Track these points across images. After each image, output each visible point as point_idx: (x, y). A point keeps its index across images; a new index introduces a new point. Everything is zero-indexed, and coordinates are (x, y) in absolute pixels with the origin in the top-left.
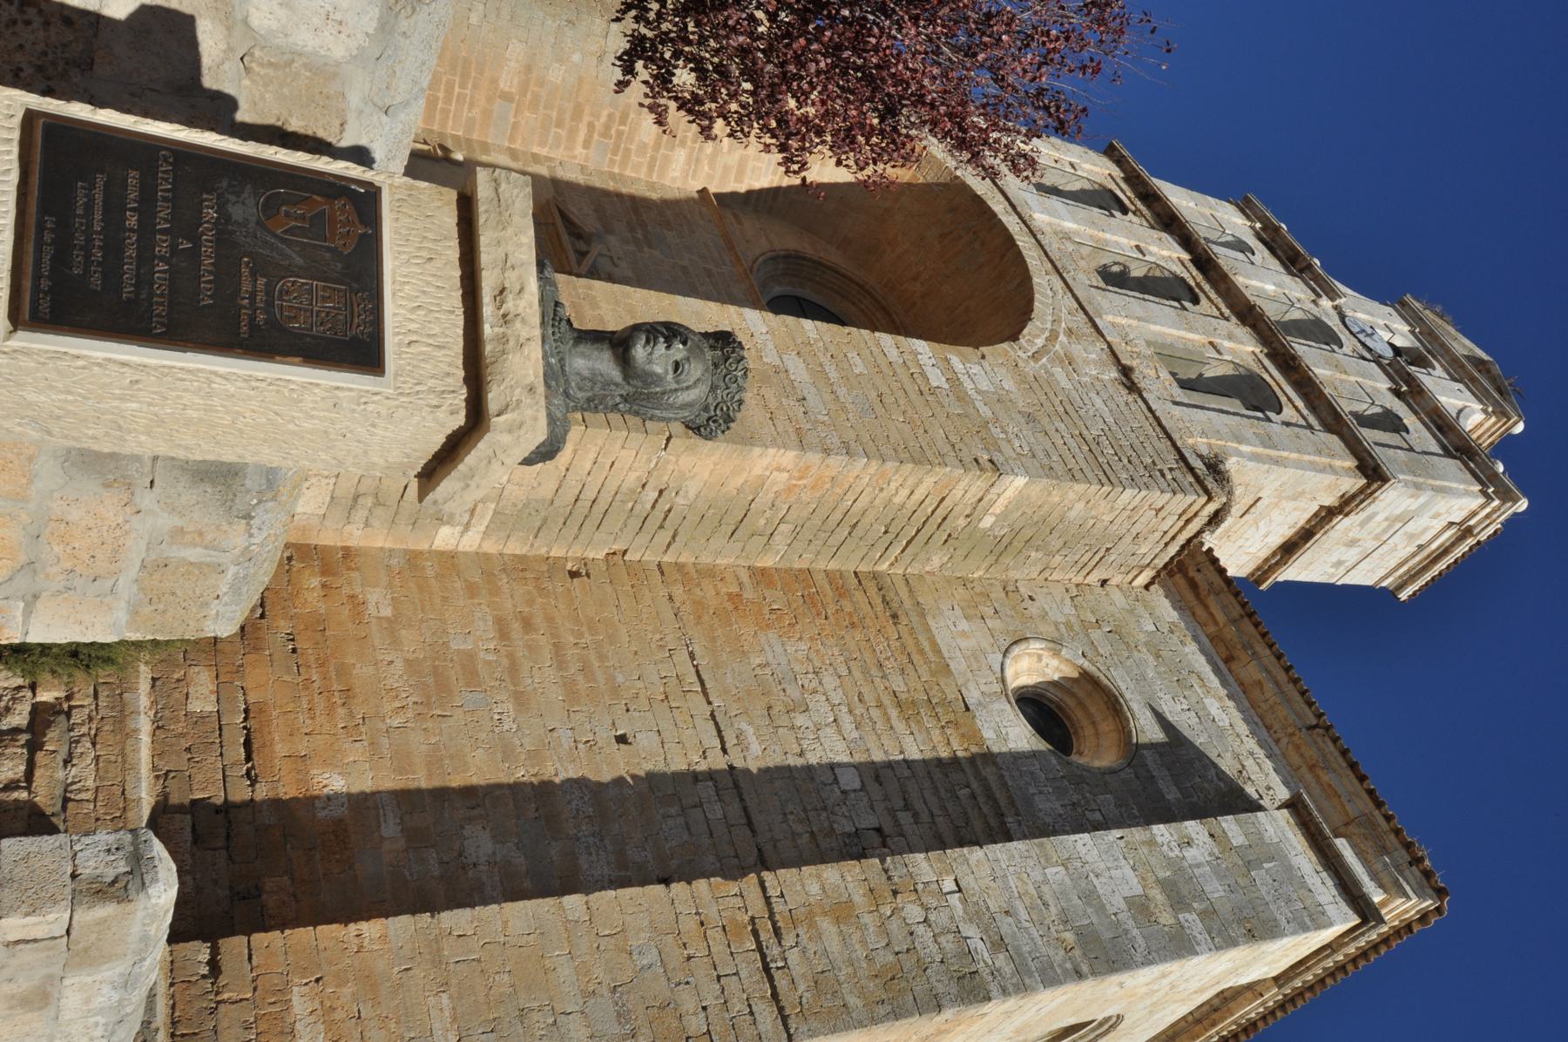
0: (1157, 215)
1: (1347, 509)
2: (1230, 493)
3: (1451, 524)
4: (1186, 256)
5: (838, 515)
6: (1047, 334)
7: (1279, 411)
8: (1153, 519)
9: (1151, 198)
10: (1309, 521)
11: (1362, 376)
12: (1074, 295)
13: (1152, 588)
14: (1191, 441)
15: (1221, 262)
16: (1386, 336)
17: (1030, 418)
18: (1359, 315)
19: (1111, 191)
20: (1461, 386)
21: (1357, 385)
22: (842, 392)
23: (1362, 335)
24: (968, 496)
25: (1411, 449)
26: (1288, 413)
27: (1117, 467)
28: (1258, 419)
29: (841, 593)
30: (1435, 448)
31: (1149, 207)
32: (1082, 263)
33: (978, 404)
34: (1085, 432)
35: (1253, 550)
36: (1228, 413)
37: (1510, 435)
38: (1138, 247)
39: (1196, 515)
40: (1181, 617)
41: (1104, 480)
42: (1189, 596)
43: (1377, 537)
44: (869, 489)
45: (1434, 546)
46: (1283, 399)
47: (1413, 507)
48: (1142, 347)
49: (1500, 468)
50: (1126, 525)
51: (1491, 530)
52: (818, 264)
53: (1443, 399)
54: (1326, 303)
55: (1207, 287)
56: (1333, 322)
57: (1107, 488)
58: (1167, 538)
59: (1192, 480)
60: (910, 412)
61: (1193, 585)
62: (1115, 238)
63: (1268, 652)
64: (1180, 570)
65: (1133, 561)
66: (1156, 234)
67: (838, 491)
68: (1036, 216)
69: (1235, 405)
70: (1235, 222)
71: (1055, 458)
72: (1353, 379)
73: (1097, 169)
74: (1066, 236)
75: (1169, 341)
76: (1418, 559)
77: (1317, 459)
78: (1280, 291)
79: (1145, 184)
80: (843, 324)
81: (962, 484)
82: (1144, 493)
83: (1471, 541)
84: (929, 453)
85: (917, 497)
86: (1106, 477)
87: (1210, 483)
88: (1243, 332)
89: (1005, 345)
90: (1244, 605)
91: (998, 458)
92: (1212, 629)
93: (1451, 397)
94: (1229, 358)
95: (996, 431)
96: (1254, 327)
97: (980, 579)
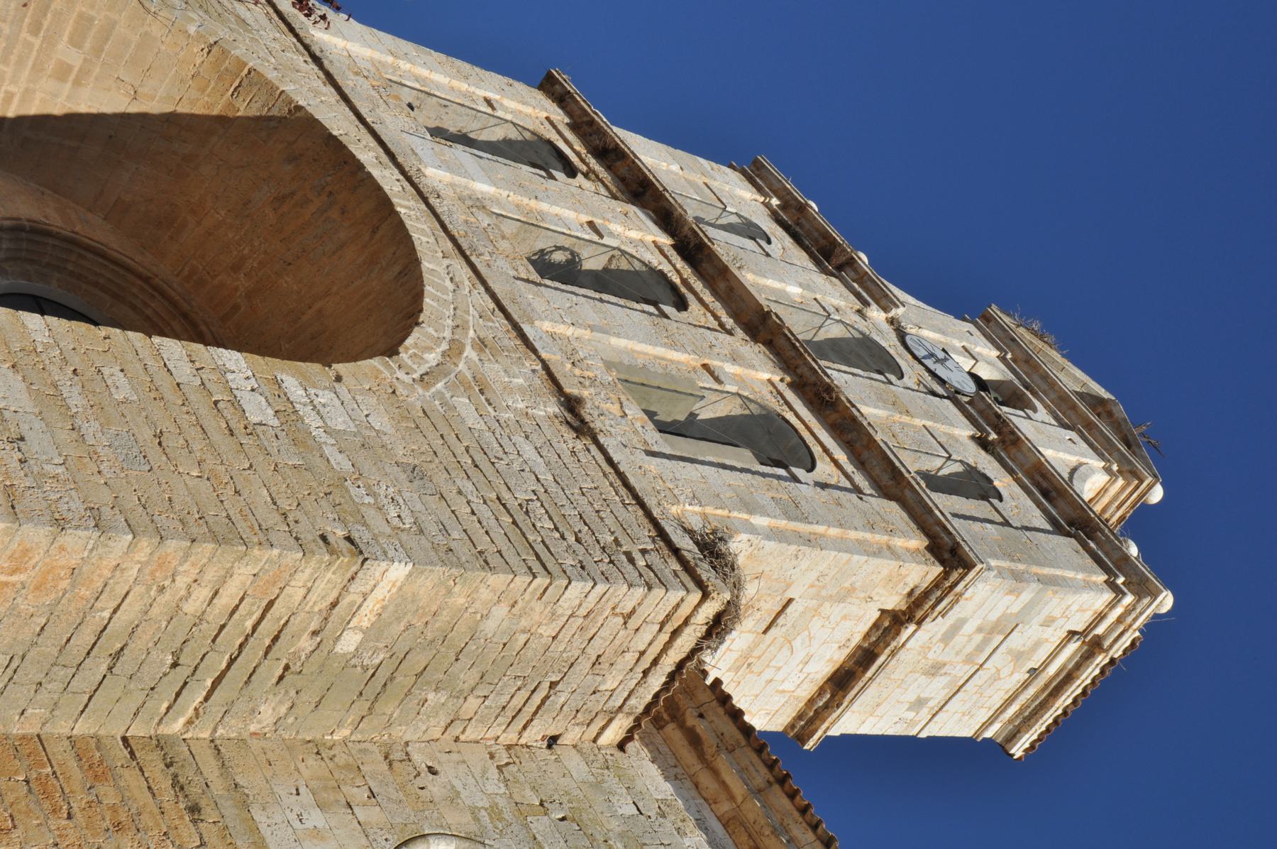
0: (621, 180)
1: (919, 614)
2: (737, 586)
3: (1072, 634)
4: (665, 240)
5: (85, 637)
6: (445, 346)
7: (811, 467)
8: (626, 628)
9: (610, 154)
10: (867, 635)
11: (932, 418)
12: (488, 290)
13: (630, 747)
14: (674, 510)
15: (719, 249)
16: (967, 364)
17: (415, 473)
18: (926, 333)
19: (550, 142)
20: (1073, 435)
21: (922, 432)
22: (90, 429)
23: (931, 362)
24: (313, 597)
25: (1006, 523)
26: (824, 469)
27: (559, 547)
28: (779, 478)
29: (98, 772)
30: (1040, 521)
31: (609, 168)
32: (503, 245)
33: (327, 451)
34: (506, 496)
35: (788, 686)
36: (732, 468)
37: (1146, 506)
38: (591, 224)
39: (686, 622)
40: (678, 790)
41: (537, 567)
42: (688, 756)
43: (969, 660)
44: (138, 589)
45: (1052, 670)
46: (817, 450)
47: (1015, 609)
48: (598, 370)
49: (1133, 550)
50: (579, 642)
51: (1126, 642)
52: (72, 242)
53: (1049, 453)
54: (875, 313)
55: (698, 285)
56: (889, 341)
57: (542, 581)
58: (646, 662)
59: (678, 567)
60: (210, 463)
61: (695, 740)
62: (555, 210)
63: (810, 836)
64: (673, 718)
65: (595, 704)
66: (620, 207)
67: (85, 592)
68: (429, 171)
69: (744, 457)
70: (743, 198)
71: (456, 534)
72: (918, 422)
73: (529, 110)
74: (479, 204)
75: (640, 361)
76: (1032, 691)
77: (868, 536)
78: (811, 295)
79: (601, 132)
80: (96, 324)
81: (302, 578)
82: (601, 588)
83: (1101, 659)
84: (242, 526)
85: (227, 599)
86: (541, 563)
87: (705, 571)
88: (754, 352)
89: (376, 362)
90: (771, 766)
91: (359, 533)
92: (725, 807)
93: (1060, 450)
94: (733, 389)
95: (358, 493)
96: (769, 344)
97: (345, 742)
